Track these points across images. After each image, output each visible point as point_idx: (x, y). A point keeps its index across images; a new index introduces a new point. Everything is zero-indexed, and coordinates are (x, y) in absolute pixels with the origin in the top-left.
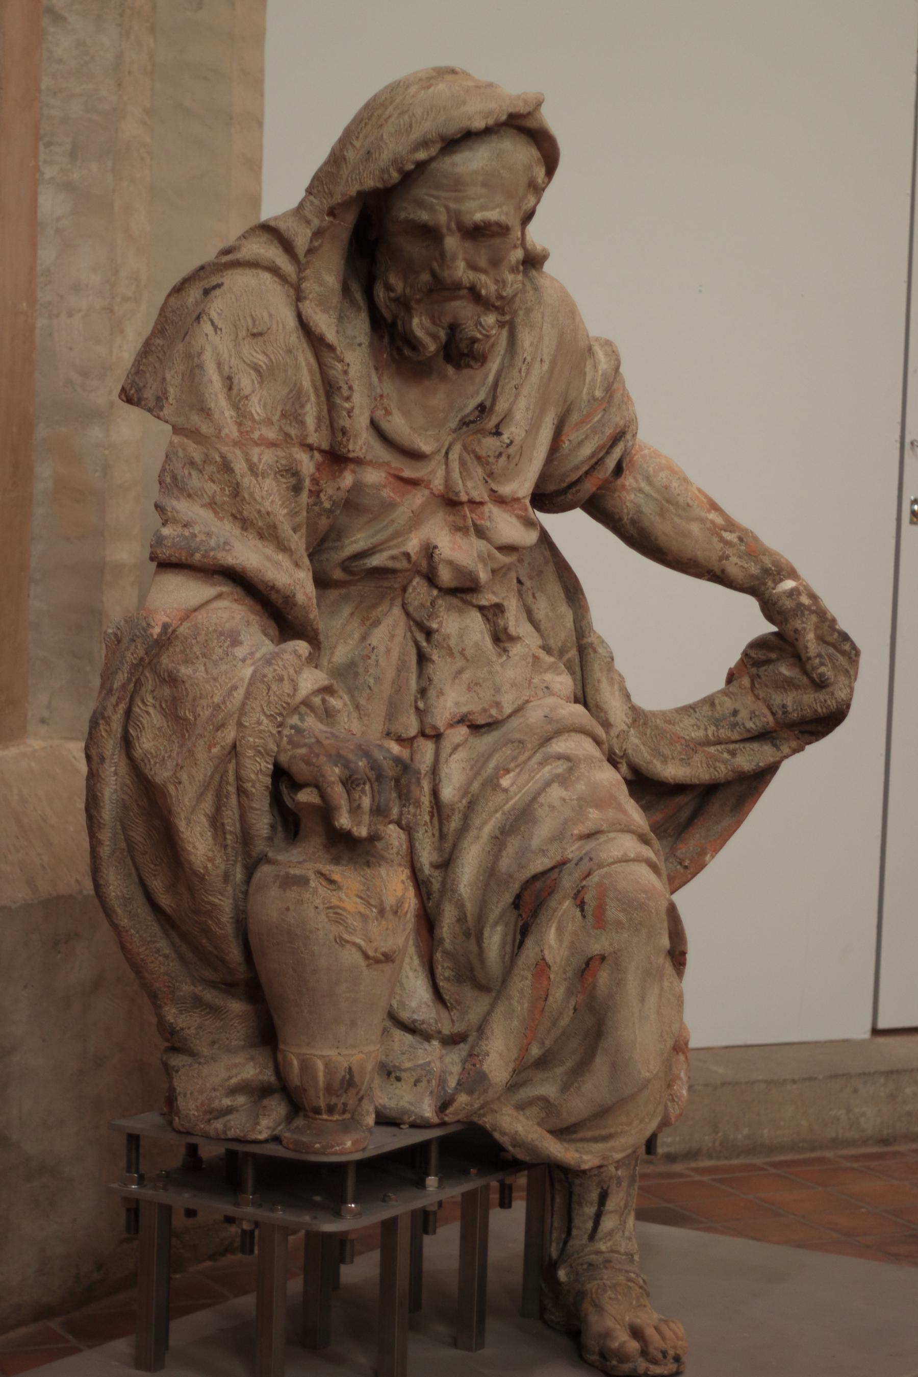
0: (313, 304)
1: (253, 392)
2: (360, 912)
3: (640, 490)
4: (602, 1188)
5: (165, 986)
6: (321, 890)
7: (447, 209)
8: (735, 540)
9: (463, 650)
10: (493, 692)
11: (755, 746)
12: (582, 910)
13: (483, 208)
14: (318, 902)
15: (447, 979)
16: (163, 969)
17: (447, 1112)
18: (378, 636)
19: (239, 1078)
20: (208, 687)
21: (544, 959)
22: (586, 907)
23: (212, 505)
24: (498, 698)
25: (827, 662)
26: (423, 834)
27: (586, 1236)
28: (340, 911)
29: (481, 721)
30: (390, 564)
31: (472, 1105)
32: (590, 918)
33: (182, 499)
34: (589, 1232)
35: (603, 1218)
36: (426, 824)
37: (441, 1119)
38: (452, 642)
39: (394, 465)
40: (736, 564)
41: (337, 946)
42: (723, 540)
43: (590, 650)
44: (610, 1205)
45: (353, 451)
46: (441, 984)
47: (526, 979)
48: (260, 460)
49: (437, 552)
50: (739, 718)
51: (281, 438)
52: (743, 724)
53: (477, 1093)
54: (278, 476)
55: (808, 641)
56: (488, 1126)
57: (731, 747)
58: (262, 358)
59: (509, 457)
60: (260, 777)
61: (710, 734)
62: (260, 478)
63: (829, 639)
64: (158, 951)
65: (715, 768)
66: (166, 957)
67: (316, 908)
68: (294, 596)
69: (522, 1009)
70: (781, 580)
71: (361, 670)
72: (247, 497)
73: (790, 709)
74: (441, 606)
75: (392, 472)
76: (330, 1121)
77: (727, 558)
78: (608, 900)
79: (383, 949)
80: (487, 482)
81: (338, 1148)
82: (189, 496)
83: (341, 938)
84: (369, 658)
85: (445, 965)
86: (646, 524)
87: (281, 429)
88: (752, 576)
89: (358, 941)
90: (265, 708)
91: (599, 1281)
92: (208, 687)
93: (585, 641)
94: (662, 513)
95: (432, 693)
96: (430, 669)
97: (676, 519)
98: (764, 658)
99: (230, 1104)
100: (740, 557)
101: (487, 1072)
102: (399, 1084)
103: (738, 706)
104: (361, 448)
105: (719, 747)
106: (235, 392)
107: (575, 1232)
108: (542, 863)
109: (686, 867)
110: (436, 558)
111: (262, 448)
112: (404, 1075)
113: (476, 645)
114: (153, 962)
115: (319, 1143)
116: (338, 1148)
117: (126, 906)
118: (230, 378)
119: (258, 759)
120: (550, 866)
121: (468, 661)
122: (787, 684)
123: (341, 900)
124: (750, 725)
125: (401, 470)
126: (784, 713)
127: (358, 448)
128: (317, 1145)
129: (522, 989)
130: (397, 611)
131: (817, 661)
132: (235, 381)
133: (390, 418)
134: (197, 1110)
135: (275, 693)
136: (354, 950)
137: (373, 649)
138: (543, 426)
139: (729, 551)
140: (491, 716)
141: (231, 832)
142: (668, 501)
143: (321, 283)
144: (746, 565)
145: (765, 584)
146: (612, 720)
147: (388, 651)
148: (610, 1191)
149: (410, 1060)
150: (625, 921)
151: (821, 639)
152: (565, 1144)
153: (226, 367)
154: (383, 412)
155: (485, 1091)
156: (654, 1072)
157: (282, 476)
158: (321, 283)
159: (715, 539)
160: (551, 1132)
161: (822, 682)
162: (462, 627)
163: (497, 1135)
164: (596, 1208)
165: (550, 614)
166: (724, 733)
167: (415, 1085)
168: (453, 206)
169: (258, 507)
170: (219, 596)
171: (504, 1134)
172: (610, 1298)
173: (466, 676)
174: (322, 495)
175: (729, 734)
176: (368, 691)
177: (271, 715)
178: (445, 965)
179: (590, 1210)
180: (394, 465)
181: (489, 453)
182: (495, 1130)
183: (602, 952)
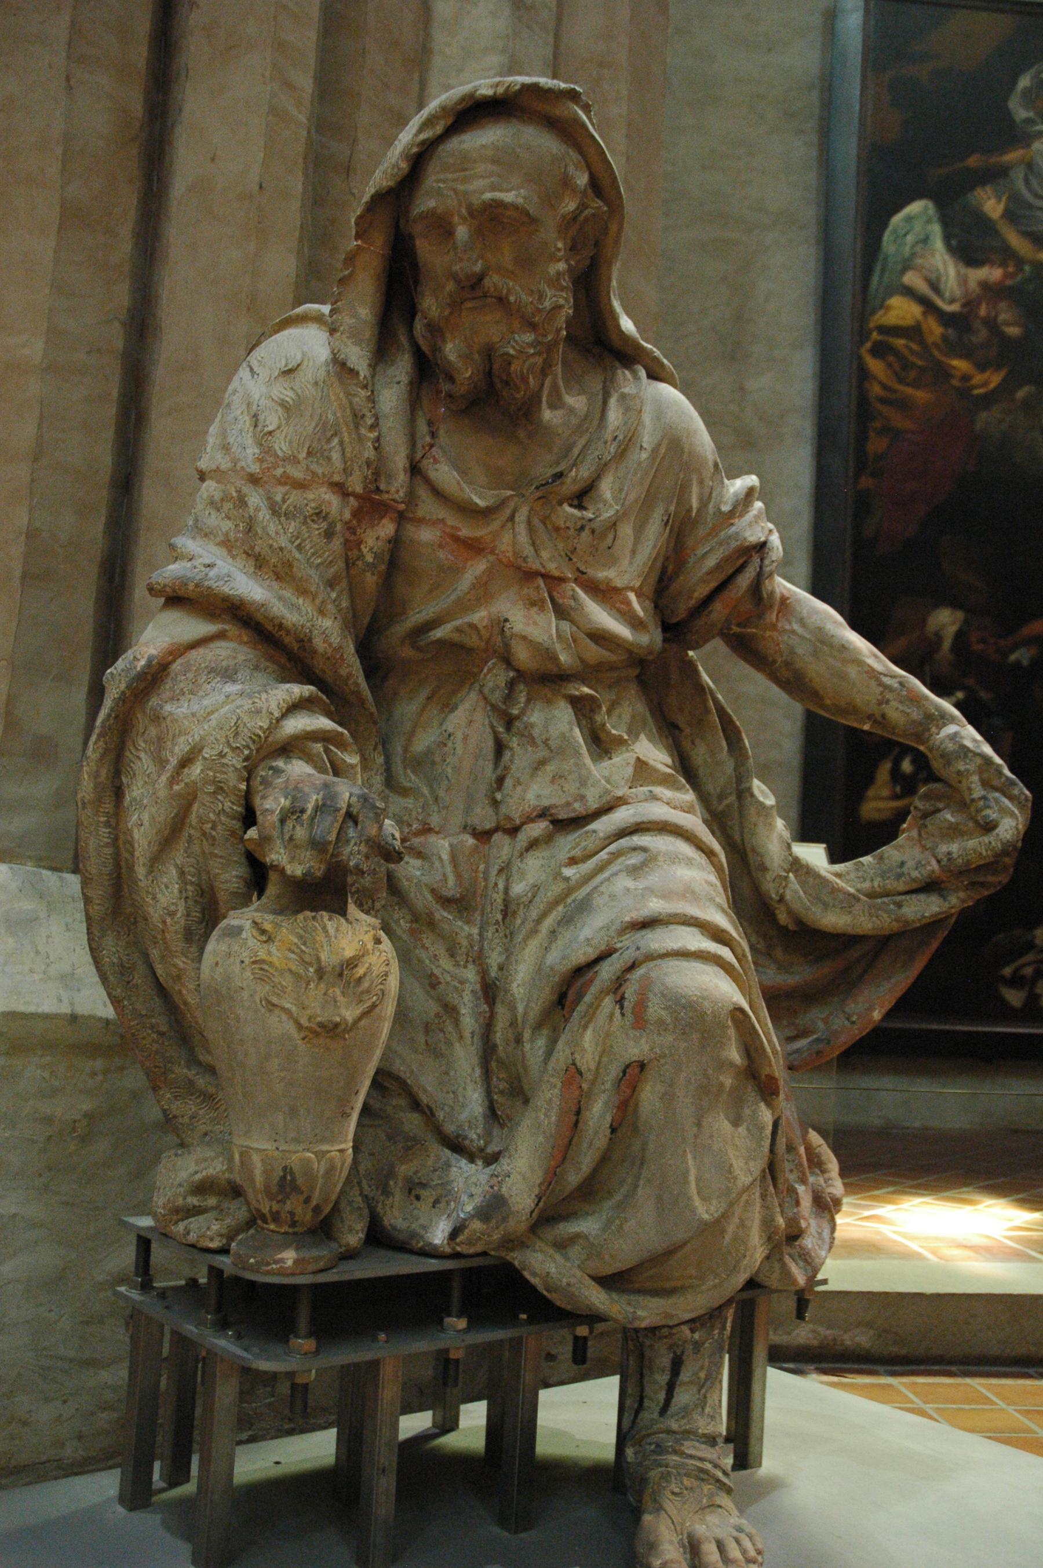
0: (344, 336)
1: (279, 428)
2: (290, 970)
3: (793, 632)
4: (675, 1353)
5: (156, 1067)
6: (251, 942)
7: (455, 190)
8: (896, 685)
9: (547, 740)
10: (578, 785)
11: (922, 897)
12: (622, 1008)
13: (493, 188)
14: (245, 955)
15: (501, 1092)
16: (155, 1047)
17: (458, 1240)
18: (456, 721)
19: (204, 1173)
20: (186, 723)
21: (574, 1064)
22: (626, 1004)
23: (226, 543)
24: (583, 791)
25: (993, 804)
26: (493, 934)
27: (658, 1409)
28: (266, 967)
29: (563, 815)
30: (456, 637)
31: (489, 1236)
32: (629, 1016)
33: (198, 538)
34: (661, 1405)
35: (677, 1390)
36: (497, 923)
37: (454, 1249)
38: (536, 732)
39: (450, 523)
40: (897, 709)
41: (263, 1010)
42: (881, 684)
43: (747, 794)
44: (685, 1376)
45: (388, 492)
46: (495, 1097)
47: (555, 1086)
48: (284, 501)
49: (508, 625)
50: (905, 870)
51: (309, 478)
52: (909, 874)
53: (494, 1221)
54: (309, 521)
55: (971, 783)
56: (516, 1263)
57: (898, 898)
58: (290, 393)
59: (593, 531)
60: (223, 818)
61: (876, 884)
62: (283, 519)
63: (996, 783)
64: (152, 1027)
65: (877, 917)
66: (161, 1034)
67: (242, 962)
68: (310, 640)
69: (549, 1123)
70: (944, 725)
71: (438, 758)
72: (259, 531)
73: (955, 855)
74: (521, 692)
75: (448, 530)
76: (278, 1232)
77: (887, 702)
78: (651, 996)
79: (319, 1019)
80: (570, 559)
81: (274, 1266)
82: (206, 535)
83: (269, 1002)
84: (445, 745)
85: (501, 1076)
86: (799, 665)
87: (308, 468)
88: (914, 721)
89: (288, 1006)
90: (231, 740)
91: (663, 1469)
92: (186, 723)
93: (743, 786)
94: (815, 654)
95: (508, 782)
96: (507, 755)
97: (831, 660)
98: (932, 808)
99: (197, 1203)
100: (901, 702)
101: (507, 1196)
102: (418, 1204)
103: (905, 858)
104: (398, 491)
105: (885, 900)
106: (259, 429)
107: (646, 1403)
108: (585, 954)
109: (853, 1023)
110: (508, 633)
111: (288, 487)
112: (424, 1193)
113: (563, 736)
114: (144, 1038)
115: (255, 1258)
116: (274, 1266)
117: (122, 974)
118: (255, 416)
119: (219, 797)
120: (593, 957)
121: (552, 751)
122: (953, 832)
123: (269, 953)
124: (915, 874)
125: (458, 529)
126: (949, 860)
127: (393, 490)
128: (252, 1260)
129: (550, 1100)
130: (473, 695)
131: (981, 803)
132: (261, 418)
133: (437, 466)
134: (164, 1208)
135: (245, 724)
136: (284, 1017)
137: (450, 735)
138: (651, 521)
139: (889, 696)
140: (575, 810)
141: (192, 883)
142: (822, 642)
143: (355, 315)
144: (908, 711)
145: (929, 730)
146: (768, 864)
147: (465, 738)
148: (684, 1357)
149: (440, 1178)
150: (669, 1021)
151: (985, 784)
152: (614, 1295)
153: (255, 407)
154: (432, 460)
155: (505, 1219)
156: (716, 1215)
157: (313, 521)
158: (355, 315)
159: (873, 683)
160: (593, 1278)
161: (987, 824)
162: (556, 720)
163: (526, 1274)
164: (668, 1377)
165: (709, 760)
166: (891, 884)
167: (434, 1207)
168: (461, 188)
169: (271, 542)
170: (220, 636)
171: (535, 1274)
172: (673, 1493)
173: (550, 768)
174: (362, 546)
175: (895, 884)
176: (446, 782)
177: (238, 748)
178: (501, 1076)
179: (663, 1379)
180: (450, 523)
181: (568, 524)
182: (524, 1269)
183: (641, 1059)
